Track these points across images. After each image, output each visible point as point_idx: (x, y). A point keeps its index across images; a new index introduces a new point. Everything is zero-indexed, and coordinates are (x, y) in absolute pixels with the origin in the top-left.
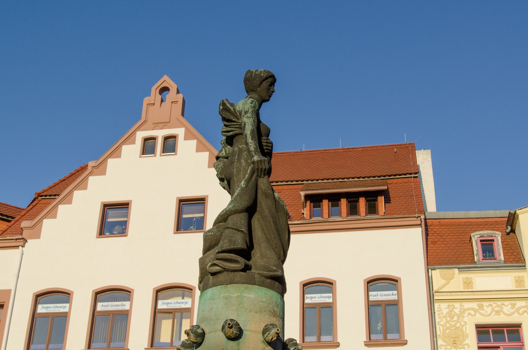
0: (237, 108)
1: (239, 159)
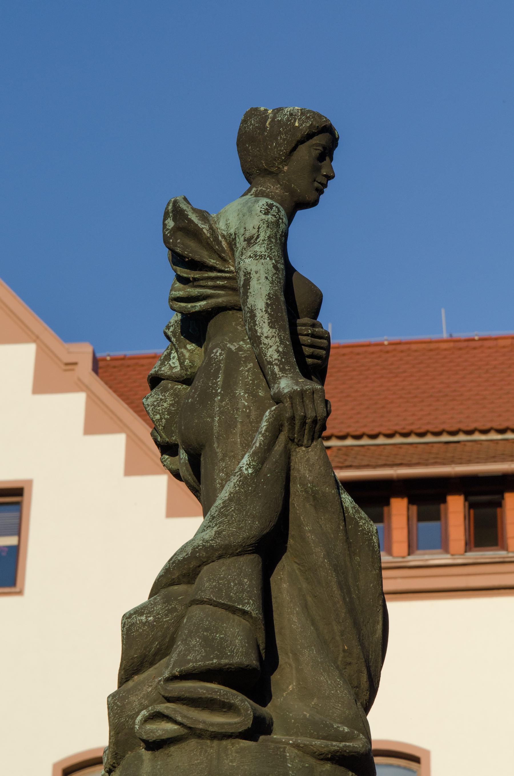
0: (221, 226)
1: (229, 386)
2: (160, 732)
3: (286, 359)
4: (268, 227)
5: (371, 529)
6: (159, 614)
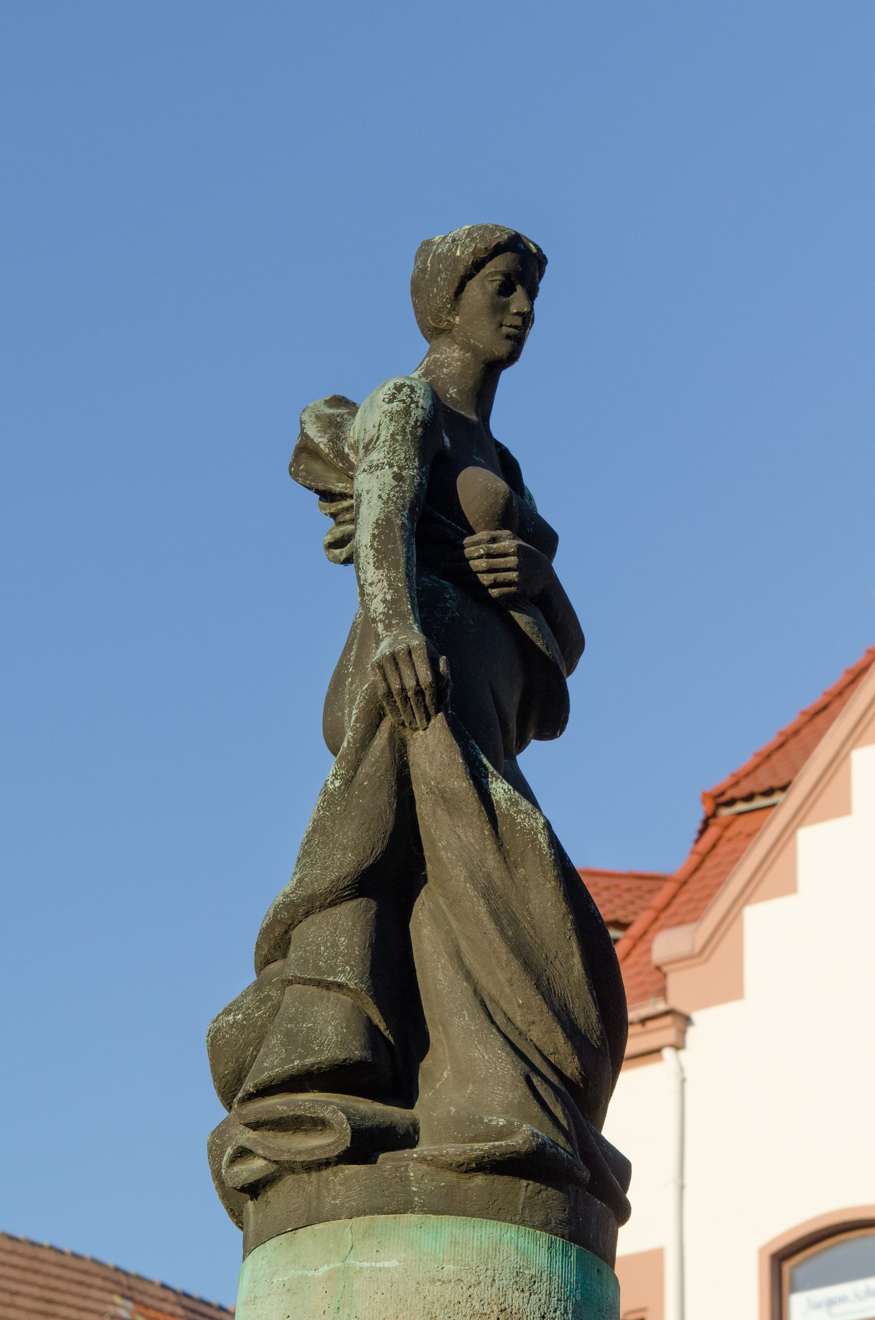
2: (245, 1174)
3: (395, 610)
4: (391, 420)
5: (534, 824)
6: (249, 1008)
